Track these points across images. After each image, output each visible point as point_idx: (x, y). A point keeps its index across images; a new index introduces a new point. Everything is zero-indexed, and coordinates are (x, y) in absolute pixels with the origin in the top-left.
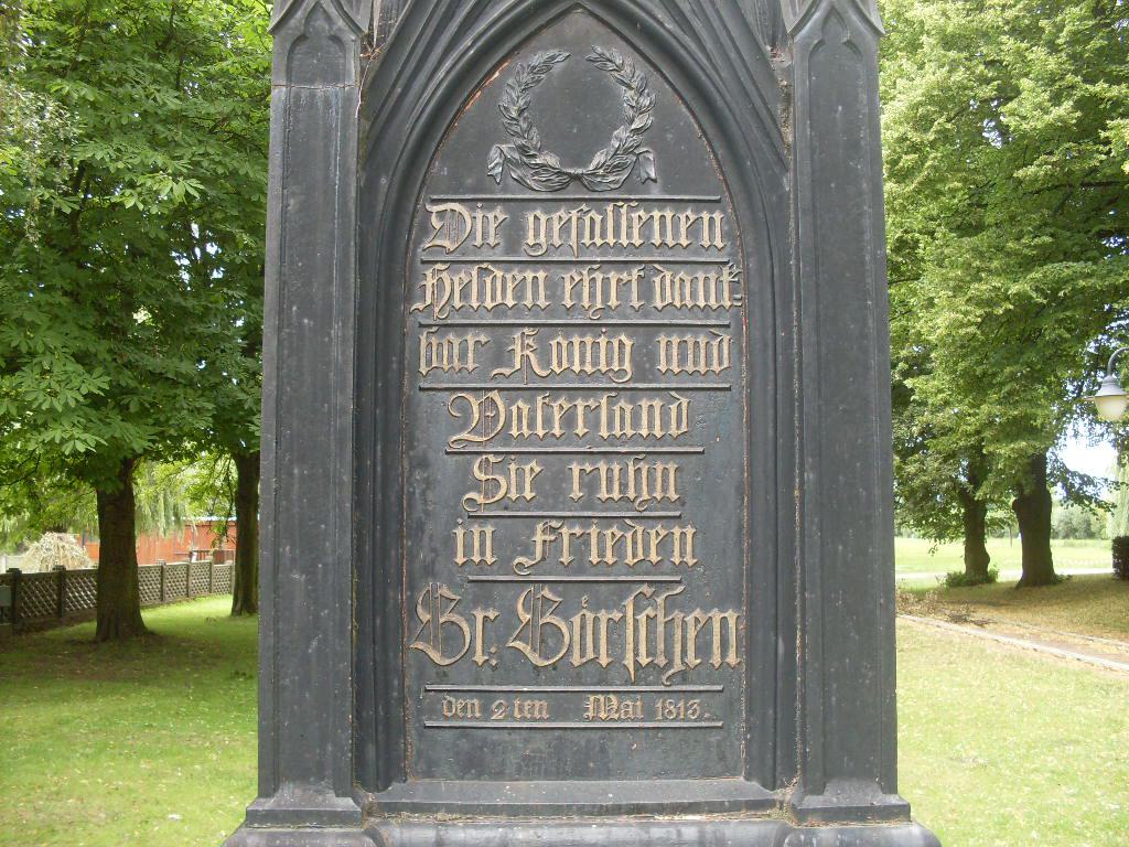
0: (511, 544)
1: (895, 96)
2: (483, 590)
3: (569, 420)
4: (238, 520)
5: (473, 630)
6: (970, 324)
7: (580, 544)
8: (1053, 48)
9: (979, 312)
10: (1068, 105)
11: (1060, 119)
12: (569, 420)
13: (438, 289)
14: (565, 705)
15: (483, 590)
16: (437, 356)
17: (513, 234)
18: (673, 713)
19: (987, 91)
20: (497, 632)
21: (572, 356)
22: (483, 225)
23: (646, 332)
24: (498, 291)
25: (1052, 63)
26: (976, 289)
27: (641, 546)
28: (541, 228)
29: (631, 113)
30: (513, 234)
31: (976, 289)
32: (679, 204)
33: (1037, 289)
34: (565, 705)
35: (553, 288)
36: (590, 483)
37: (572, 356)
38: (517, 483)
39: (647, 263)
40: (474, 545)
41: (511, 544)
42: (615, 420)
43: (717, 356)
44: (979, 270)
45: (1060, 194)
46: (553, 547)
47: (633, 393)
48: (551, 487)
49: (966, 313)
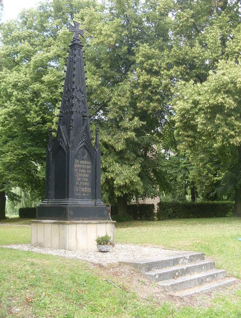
2: (78, 186)
6: (14, 160)
8: (37, 106)
9: (16, 157)
10: (40, 118)
11: (38, 120)
14: (82, 194)
15: (78, 186)
18: (88, 195)
19: (23, 112)
21: (83, 171)
24: (79, 166)
25: (37, 109)
26: (16, 152)
27: (86, 184)
28: (81, 162)
31: (16, 152)
33: (27, 153)
34: (82, 194)
37: (83, 171)
38: (80, 179)
39: (86, 165)
40: (77, 183)
42: (85, 175)
43: (90, 172)
44: (16, 148)
49: (14, 157)
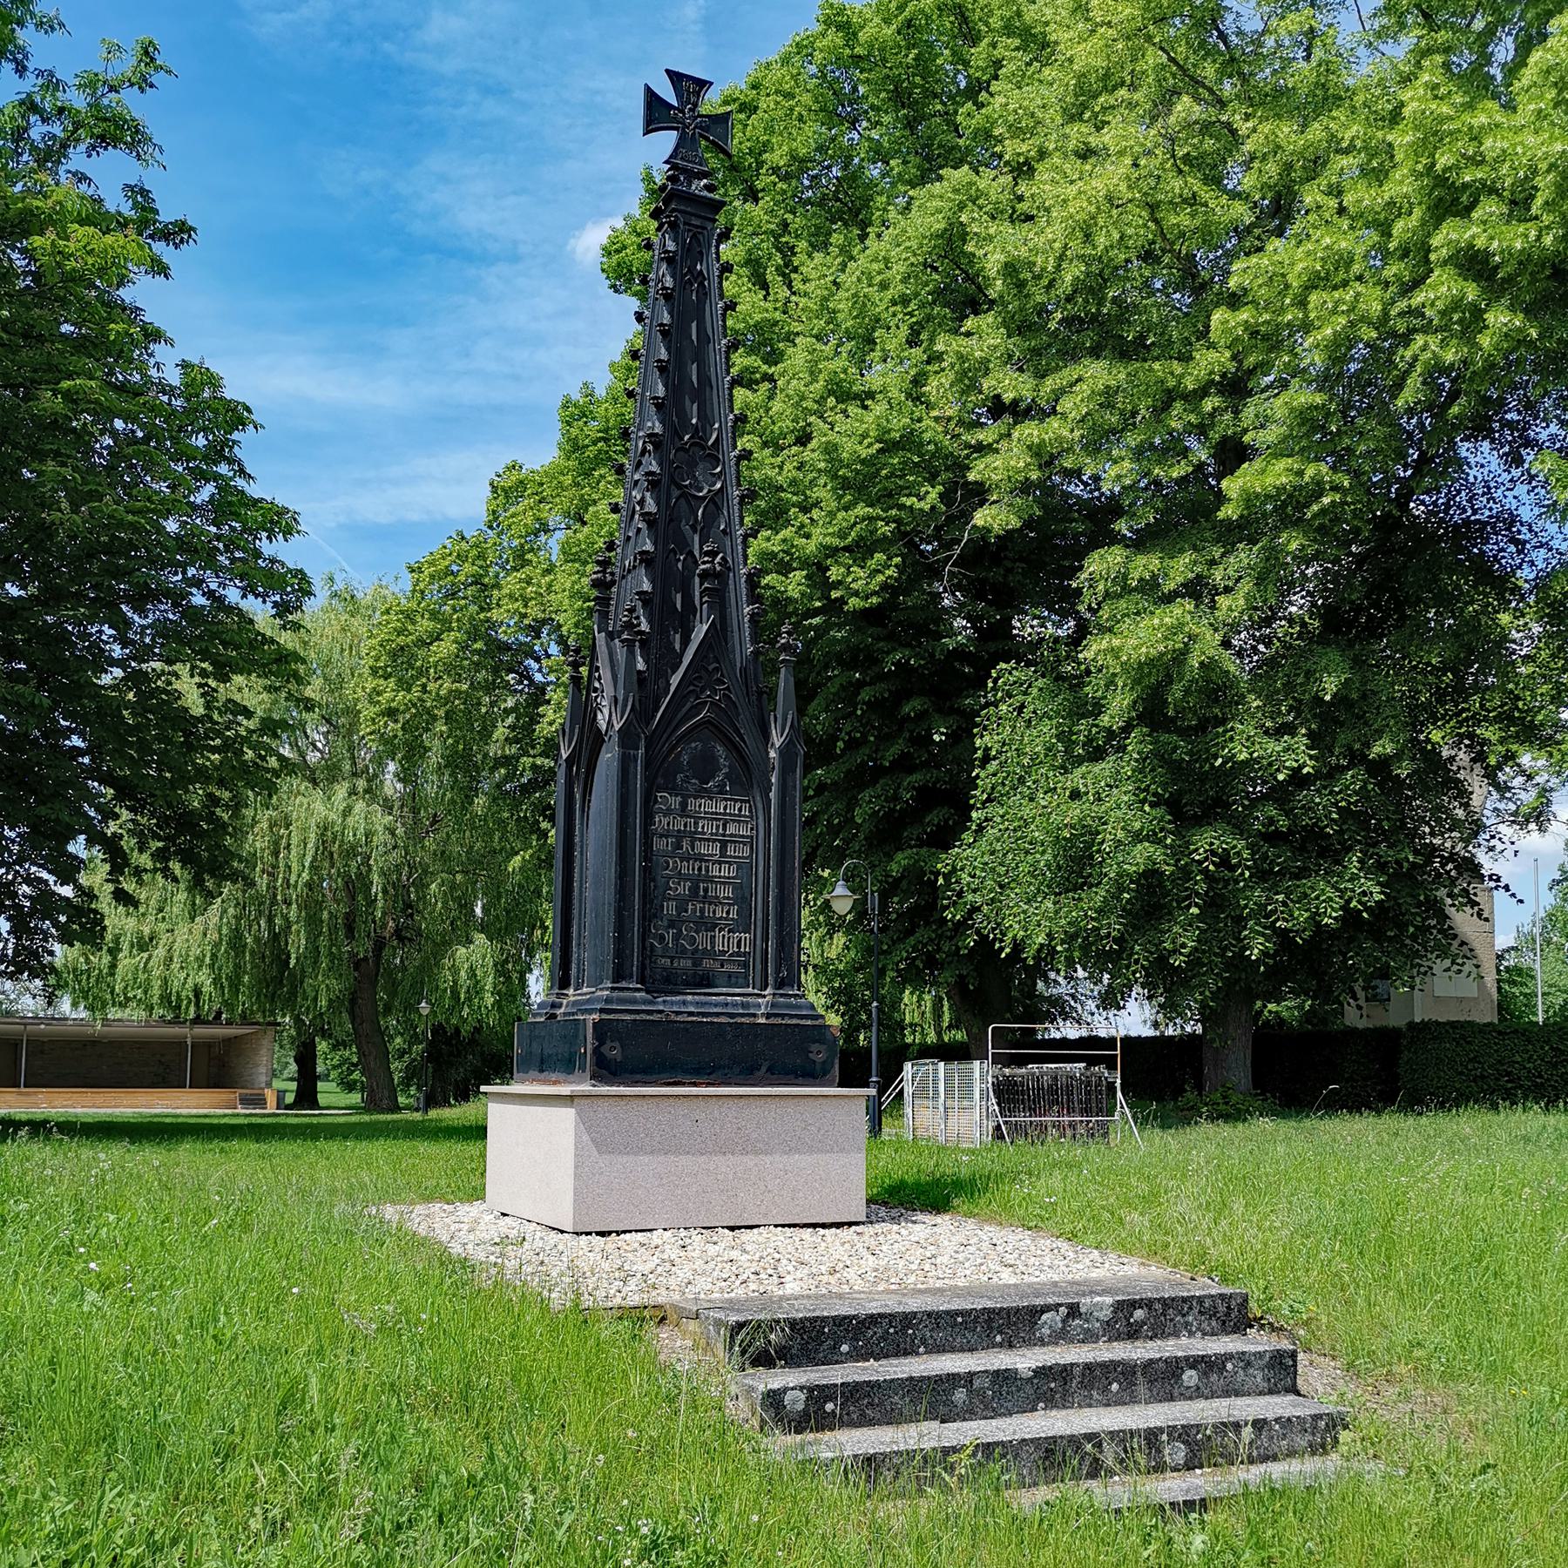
0: (682, 908)
1: (1555, 107)
2: (672, 924)
3: (700, 869)
4: (299, 1071)
5: (669, 936)
7: (702, 911)
12: (700, 869)
13: (661, 822)
16: (660, 844)
17: (684, 805)
20: (677, 937)
22: (675, 802)
23: (724, 844)
29: (1353, 779)
30: (684, 805)
32: (736, 801)
35: (696, 824)
36: (706, 890)
41: (682, 908)
45: (127, 210)
46: (694, 911)
47: (720, 863)
48: (694, 890)
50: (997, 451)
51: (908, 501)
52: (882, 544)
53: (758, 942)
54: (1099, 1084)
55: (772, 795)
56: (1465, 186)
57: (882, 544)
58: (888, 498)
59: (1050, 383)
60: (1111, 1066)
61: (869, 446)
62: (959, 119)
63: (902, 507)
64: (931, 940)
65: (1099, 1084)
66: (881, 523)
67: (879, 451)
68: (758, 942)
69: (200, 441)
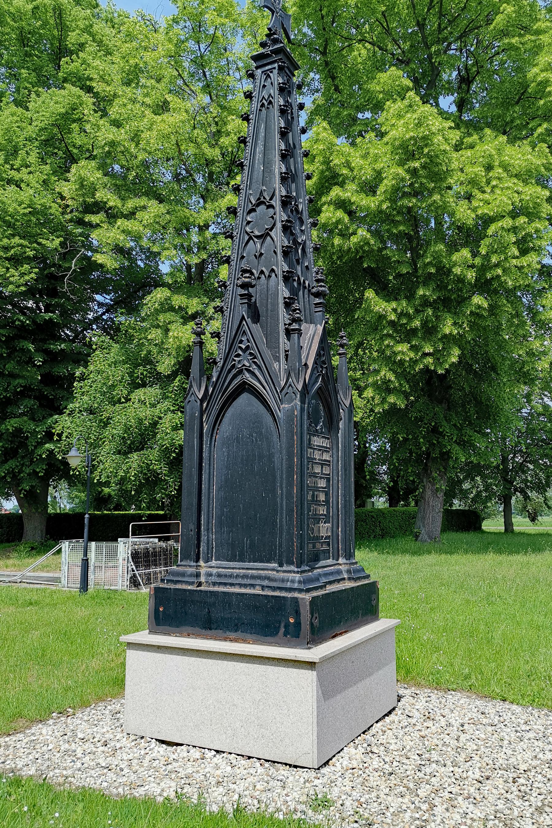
50: (101, 227)
51: (44, 242)
52: (29, 259)
53: (335, 529)
54: (171, 550)
55: (340, 435)
56: (342, 175)
57: (29, 259)
58: (32, 237)
59: (131, 204)
60: (177, 541)
61: (25, 208)
62: (61, 63)
63: (39, 244)
64: (17, 466)
65: (171, 550)
66: (28, 250)
67: (30, 212)
68: (335, 529)
69: (493, 101)
